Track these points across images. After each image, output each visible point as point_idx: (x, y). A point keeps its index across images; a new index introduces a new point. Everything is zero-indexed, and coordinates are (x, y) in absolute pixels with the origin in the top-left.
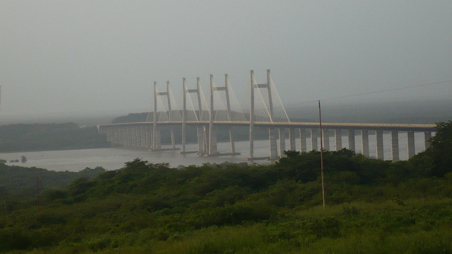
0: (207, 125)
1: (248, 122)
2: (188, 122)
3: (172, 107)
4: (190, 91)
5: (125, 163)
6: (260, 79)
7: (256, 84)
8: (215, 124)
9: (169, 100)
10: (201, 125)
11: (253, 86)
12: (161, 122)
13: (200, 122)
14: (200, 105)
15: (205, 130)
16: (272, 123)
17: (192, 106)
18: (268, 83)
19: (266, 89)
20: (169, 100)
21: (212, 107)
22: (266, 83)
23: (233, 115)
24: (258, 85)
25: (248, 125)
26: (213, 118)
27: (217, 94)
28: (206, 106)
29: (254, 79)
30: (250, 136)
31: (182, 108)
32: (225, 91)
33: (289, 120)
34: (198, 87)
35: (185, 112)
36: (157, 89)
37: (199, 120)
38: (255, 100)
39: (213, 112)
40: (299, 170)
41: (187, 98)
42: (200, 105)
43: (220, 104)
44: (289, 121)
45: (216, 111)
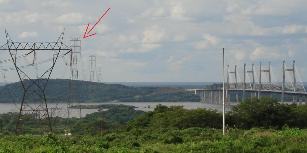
0: (257, 92)
1: (281, 91)
2: (246, 90)
3: (237, 81)
4: (248, 72)
5: (197, 108)
6: (249, 68)
7: (287, 69)
8: (261, 92)
9: (270, 75)
10: (254, 92)
11: (284, 70)
12: (231, 89)
13: (254, 90)
14: (254, 80)
15: (256, 95)
16: (295, 92)
17: (249, 80)
18: (294, 69)
19: (252, 73)
20: (270, 75)
21: (260, 82)
22: (292, 69)
23: (273, 87)
24: (287, 69)
25: (281, 93)
26: (261, 88)
27: (263, 74)
28: (257, 81)
29: (285, 66)
30: (243, 95)
31: (243, 82)
32: (268, 72)
33: (295, 91)
34: (253, 69)
35: (283, 86)
36: (246, 68)
37: (253, 89)
38: (285, 80)
39: (261, 85)
40: (111, 85)
41: (246, 75)
42: (254, 80)
43: (265, 80)
44: (305, 92)
45: (262, 85)
